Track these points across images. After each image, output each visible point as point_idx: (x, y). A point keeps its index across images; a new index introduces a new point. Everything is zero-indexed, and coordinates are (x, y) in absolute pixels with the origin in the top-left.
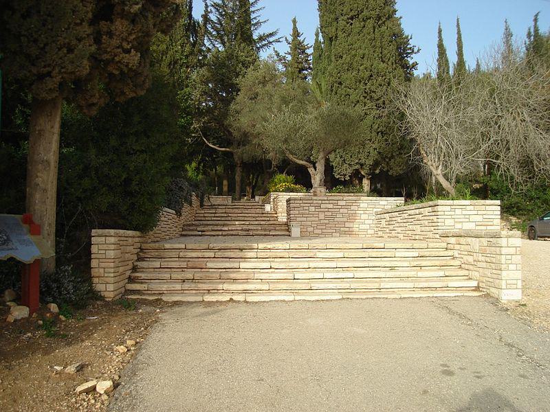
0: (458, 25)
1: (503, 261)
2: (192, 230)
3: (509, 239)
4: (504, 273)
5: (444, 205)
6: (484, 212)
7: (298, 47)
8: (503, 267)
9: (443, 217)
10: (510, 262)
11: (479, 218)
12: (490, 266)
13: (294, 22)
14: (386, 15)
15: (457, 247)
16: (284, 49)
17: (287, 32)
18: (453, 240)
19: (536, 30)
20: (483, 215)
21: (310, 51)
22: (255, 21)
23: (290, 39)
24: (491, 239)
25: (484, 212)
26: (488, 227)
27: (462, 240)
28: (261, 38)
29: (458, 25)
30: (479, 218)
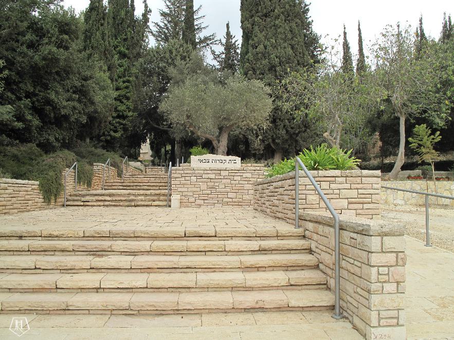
0: (359, 29)
1: (374, 277)
2: (77, 200)
3: (385, 238)
4: (375, 299)
5: (59, 153)
6: (360, 186)
7: (229, 47)
8: (374, 287)
9: (304, 192)
10: (386, 278)
11: (354, 193)
12: (354, 280)
13: (228, 25)
14: (298, 16)
15: (315, 237)
16: (219, 49)
17: (221, 36)
18: (310, 226)
19: (422, 30)
20: (204, 200)
21: (239, 51)
22: (196, 27)
23: (224, 41)
24: (355, 235)
25: (360, 186)
26: (365, 205)
27: (320, 228)
28: (201, 42)
29: (359, 29)
30: (354, 193)
